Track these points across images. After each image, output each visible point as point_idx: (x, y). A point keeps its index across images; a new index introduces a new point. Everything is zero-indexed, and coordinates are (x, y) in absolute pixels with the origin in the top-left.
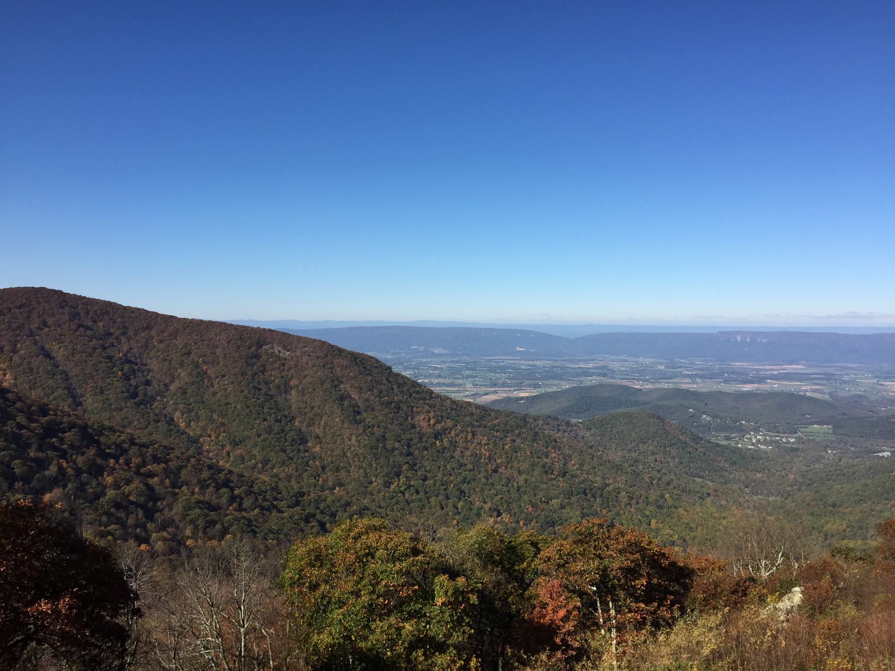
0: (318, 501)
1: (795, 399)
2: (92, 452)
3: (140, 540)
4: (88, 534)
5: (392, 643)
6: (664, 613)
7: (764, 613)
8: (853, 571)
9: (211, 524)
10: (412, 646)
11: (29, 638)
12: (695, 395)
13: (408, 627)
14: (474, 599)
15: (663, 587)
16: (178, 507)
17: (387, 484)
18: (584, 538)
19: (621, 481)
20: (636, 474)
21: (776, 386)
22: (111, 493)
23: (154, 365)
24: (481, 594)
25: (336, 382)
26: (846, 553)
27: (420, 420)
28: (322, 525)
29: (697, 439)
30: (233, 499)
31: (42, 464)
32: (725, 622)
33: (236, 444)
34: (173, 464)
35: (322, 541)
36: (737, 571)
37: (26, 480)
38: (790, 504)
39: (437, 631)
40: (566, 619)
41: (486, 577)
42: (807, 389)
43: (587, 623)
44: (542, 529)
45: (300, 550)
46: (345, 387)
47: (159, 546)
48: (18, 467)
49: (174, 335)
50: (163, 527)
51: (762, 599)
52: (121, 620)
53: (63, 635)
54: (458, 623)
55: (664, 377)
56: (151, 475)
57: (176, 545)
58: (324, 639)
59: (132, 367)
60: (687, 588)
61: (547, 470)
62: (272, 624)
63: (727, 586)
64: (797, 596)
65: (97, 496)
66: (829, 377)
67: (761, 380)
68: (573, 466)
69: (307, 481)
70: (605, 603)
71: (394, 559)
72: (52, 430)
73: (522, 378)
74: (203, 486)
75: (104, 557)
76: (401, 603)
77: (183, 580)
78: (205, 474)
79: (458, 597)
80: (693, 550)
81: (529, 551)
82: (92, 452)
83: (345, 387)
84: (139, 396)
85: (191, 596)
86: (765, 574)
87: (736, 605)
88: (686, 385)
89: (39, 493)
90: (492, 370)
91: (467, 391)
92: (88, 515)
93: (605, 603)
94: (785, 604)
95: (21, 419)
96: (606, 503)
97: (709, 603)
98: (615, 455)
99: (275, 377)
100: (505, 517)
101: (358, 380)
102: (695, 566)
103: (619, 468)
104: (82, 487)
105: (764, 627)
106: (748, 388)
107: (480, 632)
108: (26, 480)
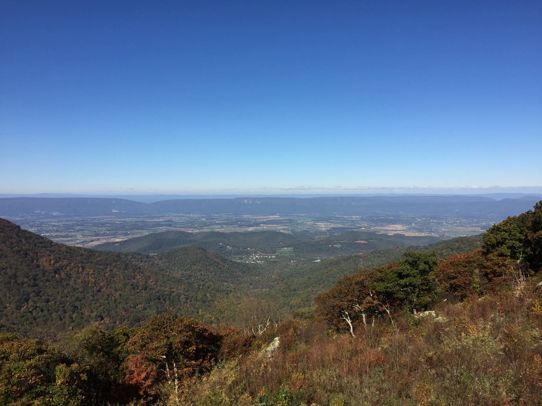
1: (275, 234)
6: (206, 364)
7: (260, 355)
12: (222, 234)
14: (84, 377)
15: (206, 348)
17: (19, 308)
21: (265, 227)
24: (89, 373)
27: (43, 262)
29: (224, 260)
32: (239, 364)
36: (246, 333)
40: (145, 379)
41: (91, 361)
42: (280, 228)
43: (160, 378)
51: (259, 347)
55: (205, 225)
60: (219, 347)
61: (134, 287)
64: (277, 342)
66: (291, 221)
67: (257, 224)
70: (171, 365)
73: (115, 229)
76: (31, 387)
79: (73, 377)
80: (223, 324)
86: (260, 333)
87: (246, 353)
88: (218, 229)
90: (96, 225)
94: (271, 348)
97: (231, 354)
98: (177, 274)
100: (107, 320)
102: (222, 333)
103: (179, 281)
105: (260, 362)
106: (251, 229)
107: (89, 397)
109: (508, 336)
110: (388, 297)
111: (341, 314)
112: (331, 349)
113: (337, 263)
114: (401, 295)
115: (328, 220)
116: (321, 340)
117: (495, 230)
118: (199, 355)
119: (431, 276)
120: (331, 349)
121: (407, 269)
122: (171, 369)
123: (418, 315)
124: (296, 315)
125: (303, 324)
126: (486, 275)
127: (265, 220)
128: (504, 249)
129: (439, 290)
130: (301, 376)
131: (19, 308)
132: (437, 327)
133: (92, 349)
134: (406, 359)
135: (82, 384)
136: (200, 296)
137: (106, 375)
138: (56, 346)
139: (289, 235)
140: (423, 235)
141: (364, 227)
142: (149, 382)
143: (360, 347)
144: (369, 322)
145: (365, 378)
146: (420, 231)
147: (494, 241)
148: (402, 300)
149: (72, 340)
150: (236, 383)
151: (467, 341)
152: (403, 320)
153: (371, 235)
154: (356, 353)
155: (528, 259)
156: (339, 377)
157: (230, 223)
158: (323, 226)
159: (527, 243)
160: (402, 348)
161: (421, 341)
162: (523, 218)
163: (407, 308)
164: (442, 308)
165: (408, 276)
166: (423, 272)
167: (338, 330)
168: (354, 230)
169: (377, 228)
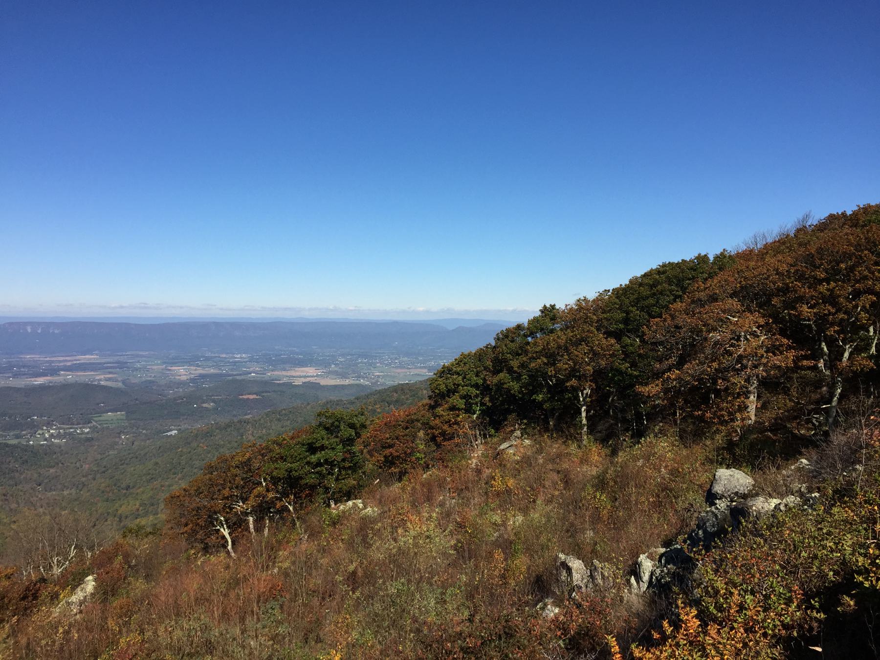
1: (89, 388)
7: (56, 611)
26: (138, 532)
32: (14, 633)
36: (29, 574)
42: (101, 378)
64: (90, 584)
66: (122, 365)
67: (54, 372)
86: (57, 571)
87: (26, 612)
94: (78, 596)
105: (55, 627)
106: (40, 381)
110: (292, 484)
111: (211, 520)
112: (193, 584)
113: (208, 434)
114: (311, 480)
117: (445, 372)
120: (193, 584)
123: (336, 509)
126: (433, 439)
127: (69, 364)
129: (369, 466)
132: (365, 524)
134: (317, 581)
139: (118, 389)
140: (347, 382)
141: (254, 371)
143: (244, 571)
144: (259, 529)
146: (344, 376)
147: (442, 390)
148: (313, 488)
151: (406, 539)
152: (314, 519)
153: (266, 386)
154: (235, 582)
156: (206, 628)
158: (182, 373)
159: (485, 389)
160: (310, 564)
161: (339, 549)
162: (480, 355)
164: (372, 492)
165: (323, 448)
167: (206, 550)
168: (238, 378)
169: (276, 373)
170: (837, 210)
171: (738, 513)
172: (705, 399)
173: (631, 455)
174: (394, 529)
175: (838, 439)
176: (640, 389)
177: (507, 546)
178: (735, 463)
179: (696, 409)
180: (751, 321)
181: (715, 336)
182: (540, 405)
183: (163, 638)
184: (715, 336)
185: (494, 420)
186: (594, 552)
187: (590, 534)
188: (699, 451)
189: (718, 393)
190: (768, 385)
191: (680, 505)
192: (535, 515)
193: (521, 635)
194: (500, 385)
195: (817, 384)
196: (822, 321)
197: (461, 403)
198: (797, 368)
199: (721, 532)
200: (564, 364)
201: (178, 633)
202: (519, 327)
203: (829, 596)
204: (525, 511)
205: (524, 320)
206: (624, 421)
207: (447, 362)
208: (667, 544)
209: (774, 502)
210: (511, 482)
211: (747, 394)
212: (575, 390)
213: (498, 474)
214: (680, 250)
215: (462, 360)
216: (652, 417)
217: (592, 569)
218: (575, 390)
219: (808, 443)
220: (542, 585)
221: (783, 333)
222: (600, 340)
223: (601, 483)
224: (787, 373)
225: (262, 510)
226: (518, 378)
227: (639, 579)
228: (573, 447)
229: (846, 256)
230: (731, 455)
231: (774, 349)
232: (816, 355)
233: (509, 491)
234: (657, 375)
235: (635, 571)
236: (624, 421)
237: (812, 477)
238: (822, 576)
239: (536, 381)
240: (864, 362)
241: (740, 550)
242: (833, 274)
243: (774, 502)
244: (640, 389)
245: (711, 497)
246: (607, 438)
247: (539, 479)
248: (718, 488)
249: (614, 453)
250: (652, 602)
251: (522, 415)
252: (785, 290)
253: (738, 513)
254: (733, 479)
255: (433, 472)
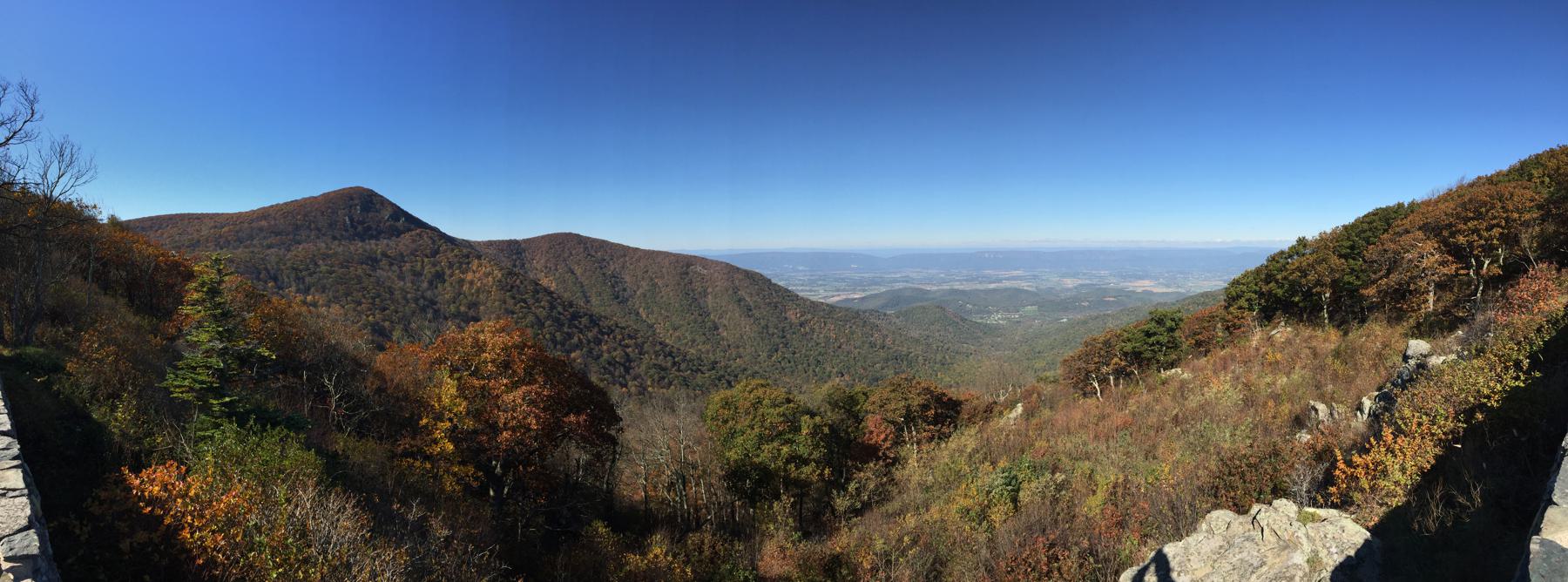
0: (726, 367)
1: (1018, 291)
2: (596, 330)
3: (623, 386)
4: (594, 379)
5: (775, 459)
6: (945, 430)
7: (1002, 422)
8: (1048, 389)
9: (662, 380)
10: (788, 462)
11: (564, 436)
12: (963, 292)
13: (785, 449)
14: (826, 430)
15: (944, 413)
16: (643, 367)
17: (770, 357)
18: (896, 388)
19: (919, 350)
20: (928, 345)
21: (1007, 284)
22: (606, 355)
23: (627, 278)
24: (831, 427)
25: (736, 290)
26: (1045, 380)
27: (790, 315)
28: (729, 383)
29: (964, 320)
30: (674, 364)
31: (570, 336)
32: (980, 431)
33: (675, 329)
34: (640, 341)
35: (728, 393)
36: (988, 399)
37: (563, 345)
38: (1016, 355)
39: (803, 450)
40: (885, 440)
41: (832, 416)
42: (1024, 285)
43: (898, 442)
44: (870, 384)
45: (717, 397)
46: (742, 293)
47: (633, 389)
48: (558, 336)
49: (638, 260)
50: (635, 379)
51: (1001, 413)
52: (613, 433)
53: (583, 437)
54: (817, 446)
55: (944, 281)
56: (627, 346)
57: (643, 390)
58: (733, 455)
59: (615, 279)
60: (958, 413)
61: (873, 345)
62: (700, 443)
63: (982, 407)
64: (1019, 408)
65: (599, 357)
66: (1035, 277)
67: (1000, 281)
68: (888, 342)
69: (719, 354)
70: (909, 428)
71: (775, 406)
72: (575, 316)
73: (856, 285)
74: (657, 354)
75: (603, 393)
76: (780, 434)
77: (647, 412)
78: (658, 348)
79: (816, 430)
80: (962, 389)
81: (862, 398)
82: (596, 330)
83: (742, 293)
84: (619, 298)
85: (652, 422)
86: (1002, 398)
87: (986, 420)
88: (957, 286)
89: (569, 352)
90: (836, 280)
91: (821, 295)
92: (594, 368)
93: (909, 428)
94: (1013, 415)
95: (560, 309)
96: (910, 365)
97: (971, 421)
98: (915, 334)
99: (697, 286)
100: (846, 377)
101: (750, 287)
102: (962, 398)
103: (917, 341)
104: (590, 351)
105: (1002, 430)
106: (992, 286)
107: (831, 452)
108: (563, 345)
109: (1247, 386)
110: (1136, 357)
111: (1087, 376)
112: (1077, 415)
113: (1085, 322)
114: (1148, 355)
115: (1075, 275)
116: (1067, 405)
117: (1236, 283)
118: (937, 420)
119: (1177, 334)
120: (1077, 415)
121: (1152, 326)
122: (910, 432)
123: (1164, 374)
124: (1040, 380)
125: (1048, 389)
126: (1228, 328)
128: (1243, 303)
129: (1184, 347)
130: (1044, 444)
131: (770, 357)
132: (1183, 384)
133: (834, 405)
134: (1153, 420)
135: (824, 437)
136: (939, 357)
137: (847, 433)
138: (801, 397)
141: (1113, 283)
142: (888, 444)
143: (1108, 411)
144: (1116, 385)
145: (1111, 443)
146: (1168, 286)
147: (1232, 296)
148: (1149, 360)
149: (815, 394)
150: (976, 451)
151: (1210, 394)
152: (1150, 380)
153: (1121, 293)
154: (1103, 417)
155: (1263, 310)
156: (1085, 444)
157: (970, 279)
158: (1070, 283)
159: (1261, 294)
160: (1148, 409)
161: (1167, 400)
162: (1258, 271)
163: (1155, 367)
164: (1187, 365)
165: (1155, 334)
166: (1171, 330)
167: (1085, 395)
170: (1483, 174)
171: (1422, 366)
172: (1403, 297)
173: (1357, 335)
174: (1202, 387)
175: (1480, 318)
176: (1365, 292)
177: (1276, 398)
178: (1420, 336)
179: (1398, 303)
180: (1430, 245)
181: (1408, 256)
182: (1297, 304)
183: (1060, 447)
184: (1408, 256)
185: (1267, 316)
186: (1332, 398)
187: (1330, 387)
188: (1400, 329)
189: (1411, 292)
190: (1441, 286)
191: (1389, 364)
192: (1295, 377)
193: (1286, 454)
194: (1270, 292)
195: (1469, 283)
196: (1470, 244)
197: (1246, 305)
198: (1457, 275)
199: (1411, 380)
200: (1312, 277)
201: (1069, 445)
202: (1282, 253)
203: (1470, 413)
204: (1288, 374)
205: (1285, 247)
206: (1353, 312)
207: (1237, 275)
208: (1379, 389)
209: (1442, 358)
210: (1279, 356)
211: (1428, 292)
212: (1319, 294)
213: (1270, 351)
214: (1387, 201)
215: (1245, 275)
216: (1371, 309)
217: (1331, 408)
218: (1319, 294)
219: (1463, 321)
220: (1299, 422)
221: (1449, 253)
222: (1335, 261)
223: (1337, 354)
224: (1451, 278)
225: (1120, 373)
226: (1282, 287)
227: (1362, 412)
228: (1319, 333)
229: (1485, 204)
230: (1419, 331)
231: (1443, 263)
232: (1468, 267)
233: (1277, 362)
234: (1374, 282)
235: (1360, 408)
236: (1353, 312)
237: (1464, 342)
238: (1467, 402)
239: (1294, 287)
240: (1496, 271)
241: (1420, 388)
242: (1479, 216)
243: (1442, 358)
244: (1365, 292)
245: (1406, 358)
246: (1342, 325)
247: (1297, 354)
248: (1409, 352)
249: (1346, 334)
250: (1370, 426)
251: (1285, 311)
252: (1450, 225)
253: (1422, 366)
254: (1418, 346)
255: (1228, 350)
